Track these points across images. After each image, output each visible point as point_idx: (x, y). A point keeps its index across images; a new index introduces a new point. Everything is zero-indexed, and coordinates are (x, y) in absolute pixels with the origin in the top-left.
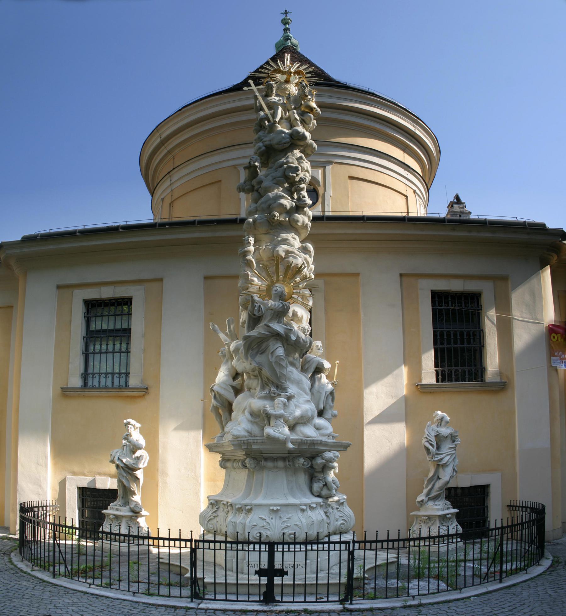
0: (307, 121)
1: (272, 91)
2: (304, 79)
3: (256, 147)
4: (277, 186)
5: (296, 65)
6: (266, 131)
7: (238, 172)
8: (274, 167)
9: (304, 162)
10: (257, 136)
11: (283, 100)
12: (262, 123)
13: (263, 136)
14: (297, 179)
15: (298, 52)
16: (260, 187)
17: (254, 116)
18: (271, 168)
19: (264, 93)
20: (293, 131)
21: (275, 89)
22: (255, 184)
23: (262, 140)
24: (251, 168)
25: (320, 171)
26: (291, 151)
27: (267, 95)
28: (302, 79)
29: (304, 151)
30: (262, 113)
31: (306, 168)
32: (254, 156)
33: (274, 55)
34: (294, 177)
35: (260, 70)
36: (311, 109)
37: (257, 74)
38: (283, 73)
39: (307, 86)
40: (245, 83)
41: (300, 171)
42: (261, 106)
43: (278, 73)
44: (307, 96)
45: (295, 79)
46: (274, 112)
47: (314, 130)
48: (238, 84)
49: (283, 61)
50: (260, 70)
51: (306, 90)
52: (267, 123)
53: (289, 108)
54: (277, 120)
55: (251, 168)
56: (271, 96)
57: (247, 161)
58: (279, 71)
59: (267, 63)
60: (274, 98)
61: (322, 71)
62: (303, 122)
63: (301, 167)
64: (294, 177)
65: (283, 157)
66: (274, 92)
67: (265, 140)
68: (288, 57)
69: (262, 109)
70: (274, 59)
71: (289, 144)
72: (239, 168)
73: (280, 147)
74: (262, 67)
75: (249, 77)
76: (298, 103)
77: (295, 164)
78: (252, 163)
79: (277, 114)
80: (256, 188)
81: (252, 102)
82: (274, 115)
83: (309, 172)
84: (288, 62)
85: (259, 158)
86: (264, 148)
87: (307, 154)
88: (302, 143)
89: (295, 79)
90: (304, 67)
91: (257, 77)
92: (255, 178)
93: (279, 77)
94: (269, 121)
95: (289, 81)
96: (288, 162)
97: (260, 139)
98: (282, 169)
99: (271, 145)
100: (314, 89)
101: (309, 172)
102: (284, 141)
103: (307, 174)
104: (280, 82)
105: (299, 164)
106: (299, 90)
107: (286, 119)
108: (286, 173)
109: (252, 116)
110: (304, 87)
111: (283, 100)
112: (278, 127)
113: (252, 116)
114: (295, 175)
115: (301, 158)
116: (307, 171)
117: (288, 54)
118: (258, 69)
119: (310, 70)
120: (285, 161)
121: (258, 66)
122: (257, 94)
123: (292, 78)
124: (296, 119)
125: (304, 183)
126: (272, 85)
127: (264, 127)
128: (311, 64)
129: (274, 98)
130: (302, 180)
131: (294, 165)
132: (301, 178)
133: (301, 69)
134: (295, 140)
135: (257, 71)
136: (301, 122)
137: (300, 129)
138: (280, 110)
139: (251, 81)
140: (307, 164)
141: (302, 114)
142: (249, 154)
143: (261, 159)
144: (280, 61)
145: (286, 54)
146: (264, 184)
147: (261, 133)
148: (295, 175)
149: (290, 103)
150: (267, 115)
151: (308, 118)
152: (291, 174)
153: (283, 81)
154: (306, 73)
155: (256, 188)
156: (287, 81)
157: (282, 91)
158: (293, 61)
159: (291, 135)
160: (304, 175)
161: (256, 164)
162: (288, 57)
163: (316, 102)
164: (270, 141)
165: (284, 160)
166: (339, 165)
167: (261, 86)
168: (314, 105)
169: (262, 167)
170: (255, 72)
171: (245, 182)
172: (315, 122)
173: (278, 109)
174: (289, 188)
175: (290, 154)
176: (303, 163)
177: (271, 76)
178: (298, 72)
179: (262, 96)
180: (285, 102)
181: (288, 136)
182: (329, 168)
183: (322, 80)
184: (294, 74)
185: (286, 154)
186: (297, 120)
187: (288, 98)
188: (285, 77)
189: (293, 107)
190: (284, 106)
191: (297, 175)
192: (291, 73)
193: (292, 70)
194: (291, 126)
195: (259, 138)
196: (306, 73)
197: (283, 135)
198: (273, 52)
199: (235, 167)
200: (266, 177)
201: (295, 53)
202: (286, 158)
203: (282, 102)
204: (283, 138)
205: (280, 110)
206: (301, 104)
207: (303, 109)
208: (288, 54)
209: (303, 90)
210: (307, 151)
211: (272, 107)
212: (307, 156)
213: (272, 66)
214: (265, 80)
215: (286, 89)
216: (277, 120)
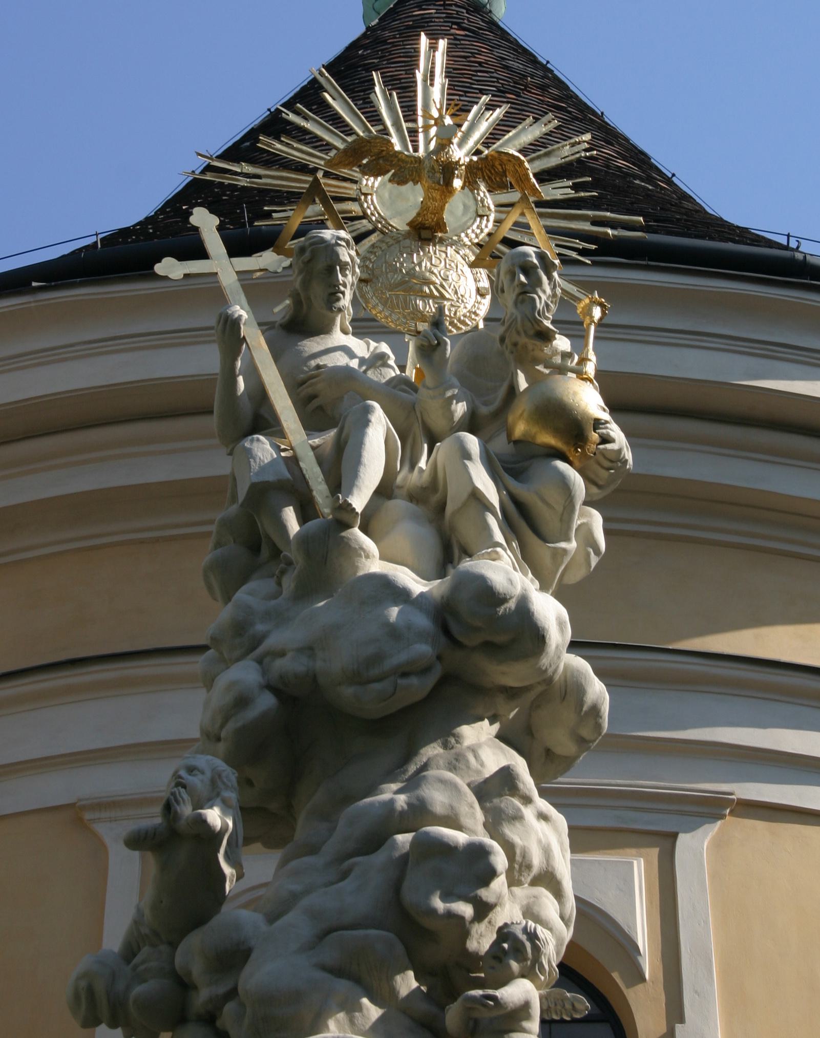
0: (548, 518)
1: (333, 295)
2: (531, 219)
3: (220, 695)
4: (343, 986)
5: (483, 120)
6: (289, 583)
7: (100, 850)
8: (330, 849)
9: (528, 813)
10: (225, 614)
11: (398, 363)
12: (265, 525)
13: (268, 615)
14: (482, 940)
15: (493, 25)
16: (233, 993)
17: (213, 464)
18: (313, 850)
19: (281, 309)
20: (456, 588)
21: (348, 281)
22: (197, 971)
23: (257, 641)
24: (177, 845)
25: (640, 868)
26: (446, 733)
27: (301, 323)
28: (514, 216)
29: (529, 731)
30: (263, 449)
31: (537, 860)
32: (202, 761)
33: (354, 46)
34: (461, 927)
35: (266, 143)
36: (574, 429)
37: (244, 173)
38: (404, 171)
39: (548, 267)
40: (168, 231)
41: (499, 884)
42: (260, 395)
43: (377, 172)
44: (545, 336)
45: (474, 215)
46: (340, 446)
47: (592, 577)
48: (124, 233)
49: (404, 88)
50: (266, 143)
51: (544, 296)
52: (290, 516)
53: (437, 422)
54: (359, 501)
55: (177, 845)
56: (325, 329)
57: (156, 777)
58: (374, 156)
59: (310, 96)
60: (343, 347)
61: (640, 158)
62: (527, 524)
63: (509, 848)
64: (461, 927)
65: (390, 776)
66: (346, 301)
67: (274, 641)
68: (433, 57)
69: (263, 421)
70: (350, 69)
71: (431, 681)
72: (101, 829)
73: (369, 700)
74: (274, 125)
75: (196, 192)
76: (492, 378)
77: (468, 831)
78: (186, 810)
79: (357, 461)
80: (203, 996)
81: (204, 360)
82: (340, 465)
83: (558, 892)
84: (437, 93)
85: (230, 775)
86: (266, 702)
87: (549, 753)
88: (511, 674)
89: (474, 215)
90: (530, 132)
91: (248, 193)
92: (199, 920)
93: (384, 200)
94: (306, 512)
95: (440, 226)
96: (419, 813)
97: (243, 638)
98: (379, 858)
99: (312, 678)
100: (587, 286)
101: (558, 892)
102: (400, 657)
103: (549, 906)
104: (380, 229)
105: (494, 825)
106: (497, 290)
107: (417, 496)
108: (409, 895)
109: (194, 459)
110: (528, 269)
111: (398, 363)
112: (359, 551)
113: (194, 459)
114: (466, 910)
115: (505, 779)
116: (548, 879)
117: (434, 38)
118: (252, 135)
119: (565, 152)
120: (402, 800)
121: (255, 115)
122: (241, 311)
123: (455, 210)
124: (476, 496)
125: (528, 973)
126: (330, 249)
127: (276, 553)
128: (576, 113)
129: (343, 347)
130: (514, 949)
131: (460, 838)
132: (504, 934)
133: (513, 144)
134: (473, 653)
135: (244, 149)
136: (508, 524)
137: (502, 569)
138: (378, 431)
139: (204, 221)
140: (543, 832)
141: (512, 465)
142: (161, 733)
143: (246, 782)
144: (390, 82)
145: (424, 41)
146: (258, 975)
147: (253, 594)
148: (466, 910)
149: (443, 385)
150: (293, 462)
151: (554, 496)
152: (439, 904)
153: (400, 224)
154: (544, 176)
155: (203, 996)
156: (427, 230)
157: (395, 297)
158: (460, 98)
159: (444, 615)
160: (529, 912)
161: (214, 816)
162: (433, 57)
163: (607, 382)
164: (309, 650)
165: (392, 794)
166: (760, 826)
167: (268, 259)
168: (589, 400)
169: (248, 841)
170: (233, 153)
171: (130, 952)
172: (596, 520)
173: (365, 423)
174: (424, 1007)
175: (433, 750)
176: (518, 817)
177: (330, 186)
178: (491, 171)
179: (265, 326)
180: (411, 373)
181: (422, 621)
182: (696, 846)
183: (638, 220)
184: (471, 184)
185: (410, 754)
186: (486, 506)
187: (430, 350)
188: (414, 196)
189: (460, 409)
190: (403, 401)
191: (483, 910)
192: (449, 169)
193: (460, 154)
194: (448, 551)
195: (240, 627)
196: (544, 176)
197: (394, 612)
198: (348, 25)
199: (76, 816)
200: (271, 918)
201: (476, 34)
202: (414, 783)
203: (392, 373)
204: (394, 632)
205: (378, 431)
206: (512, 390)
207: (520, 429)
208: (434, 38)
209: (525, 294)
210: (542, 725)
211: (330, 404)
212: (545, 763)
213: (336, 120)
214: (291, 217)
215: (415, 284)
216: (359, 501)
